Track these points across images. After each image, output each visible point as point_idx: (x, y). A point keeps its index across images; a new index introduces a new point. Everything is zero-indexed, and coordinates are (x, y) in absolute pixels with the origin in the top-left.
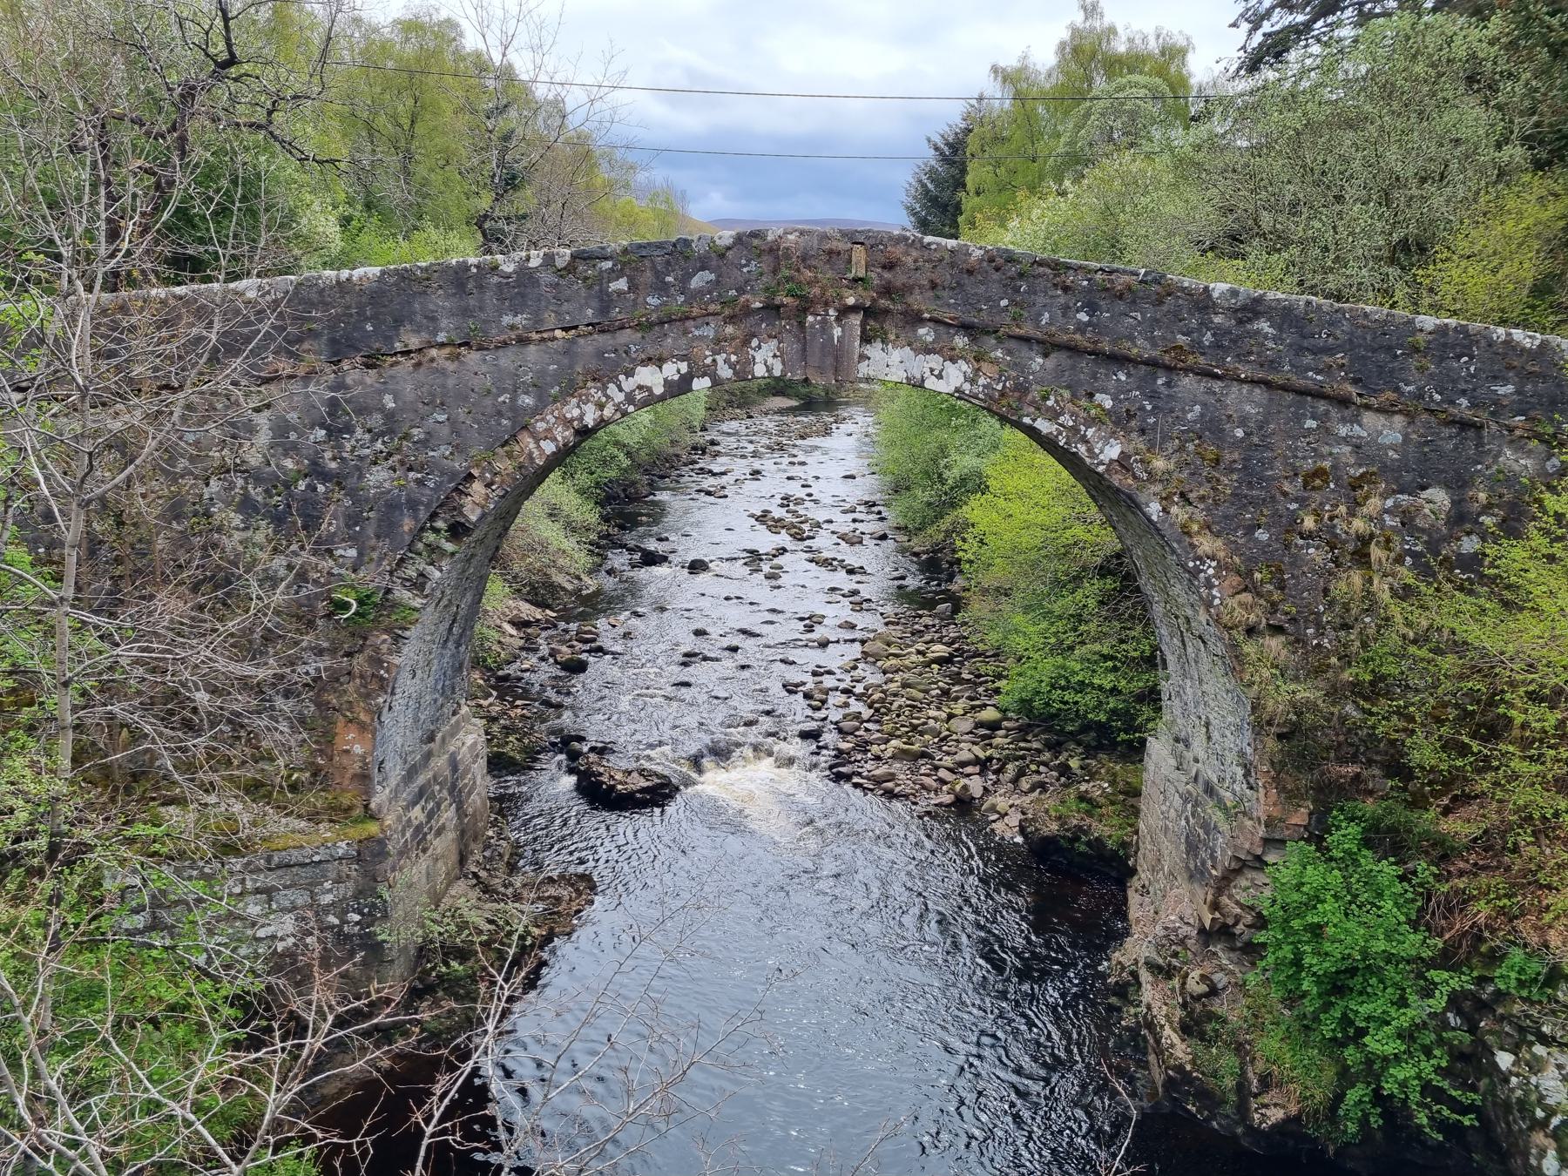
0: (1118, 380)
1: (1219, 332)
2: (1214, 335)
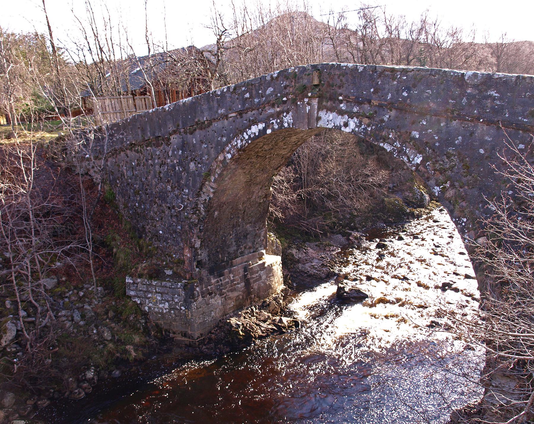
0: (423, 124)
1: (470, 97)
2: (467, 99)
